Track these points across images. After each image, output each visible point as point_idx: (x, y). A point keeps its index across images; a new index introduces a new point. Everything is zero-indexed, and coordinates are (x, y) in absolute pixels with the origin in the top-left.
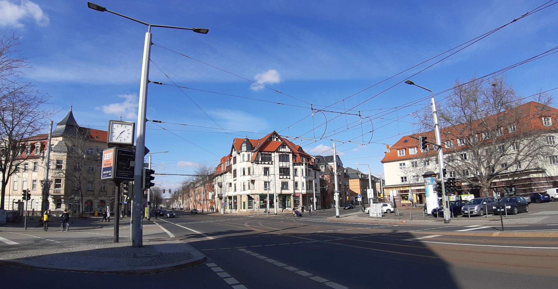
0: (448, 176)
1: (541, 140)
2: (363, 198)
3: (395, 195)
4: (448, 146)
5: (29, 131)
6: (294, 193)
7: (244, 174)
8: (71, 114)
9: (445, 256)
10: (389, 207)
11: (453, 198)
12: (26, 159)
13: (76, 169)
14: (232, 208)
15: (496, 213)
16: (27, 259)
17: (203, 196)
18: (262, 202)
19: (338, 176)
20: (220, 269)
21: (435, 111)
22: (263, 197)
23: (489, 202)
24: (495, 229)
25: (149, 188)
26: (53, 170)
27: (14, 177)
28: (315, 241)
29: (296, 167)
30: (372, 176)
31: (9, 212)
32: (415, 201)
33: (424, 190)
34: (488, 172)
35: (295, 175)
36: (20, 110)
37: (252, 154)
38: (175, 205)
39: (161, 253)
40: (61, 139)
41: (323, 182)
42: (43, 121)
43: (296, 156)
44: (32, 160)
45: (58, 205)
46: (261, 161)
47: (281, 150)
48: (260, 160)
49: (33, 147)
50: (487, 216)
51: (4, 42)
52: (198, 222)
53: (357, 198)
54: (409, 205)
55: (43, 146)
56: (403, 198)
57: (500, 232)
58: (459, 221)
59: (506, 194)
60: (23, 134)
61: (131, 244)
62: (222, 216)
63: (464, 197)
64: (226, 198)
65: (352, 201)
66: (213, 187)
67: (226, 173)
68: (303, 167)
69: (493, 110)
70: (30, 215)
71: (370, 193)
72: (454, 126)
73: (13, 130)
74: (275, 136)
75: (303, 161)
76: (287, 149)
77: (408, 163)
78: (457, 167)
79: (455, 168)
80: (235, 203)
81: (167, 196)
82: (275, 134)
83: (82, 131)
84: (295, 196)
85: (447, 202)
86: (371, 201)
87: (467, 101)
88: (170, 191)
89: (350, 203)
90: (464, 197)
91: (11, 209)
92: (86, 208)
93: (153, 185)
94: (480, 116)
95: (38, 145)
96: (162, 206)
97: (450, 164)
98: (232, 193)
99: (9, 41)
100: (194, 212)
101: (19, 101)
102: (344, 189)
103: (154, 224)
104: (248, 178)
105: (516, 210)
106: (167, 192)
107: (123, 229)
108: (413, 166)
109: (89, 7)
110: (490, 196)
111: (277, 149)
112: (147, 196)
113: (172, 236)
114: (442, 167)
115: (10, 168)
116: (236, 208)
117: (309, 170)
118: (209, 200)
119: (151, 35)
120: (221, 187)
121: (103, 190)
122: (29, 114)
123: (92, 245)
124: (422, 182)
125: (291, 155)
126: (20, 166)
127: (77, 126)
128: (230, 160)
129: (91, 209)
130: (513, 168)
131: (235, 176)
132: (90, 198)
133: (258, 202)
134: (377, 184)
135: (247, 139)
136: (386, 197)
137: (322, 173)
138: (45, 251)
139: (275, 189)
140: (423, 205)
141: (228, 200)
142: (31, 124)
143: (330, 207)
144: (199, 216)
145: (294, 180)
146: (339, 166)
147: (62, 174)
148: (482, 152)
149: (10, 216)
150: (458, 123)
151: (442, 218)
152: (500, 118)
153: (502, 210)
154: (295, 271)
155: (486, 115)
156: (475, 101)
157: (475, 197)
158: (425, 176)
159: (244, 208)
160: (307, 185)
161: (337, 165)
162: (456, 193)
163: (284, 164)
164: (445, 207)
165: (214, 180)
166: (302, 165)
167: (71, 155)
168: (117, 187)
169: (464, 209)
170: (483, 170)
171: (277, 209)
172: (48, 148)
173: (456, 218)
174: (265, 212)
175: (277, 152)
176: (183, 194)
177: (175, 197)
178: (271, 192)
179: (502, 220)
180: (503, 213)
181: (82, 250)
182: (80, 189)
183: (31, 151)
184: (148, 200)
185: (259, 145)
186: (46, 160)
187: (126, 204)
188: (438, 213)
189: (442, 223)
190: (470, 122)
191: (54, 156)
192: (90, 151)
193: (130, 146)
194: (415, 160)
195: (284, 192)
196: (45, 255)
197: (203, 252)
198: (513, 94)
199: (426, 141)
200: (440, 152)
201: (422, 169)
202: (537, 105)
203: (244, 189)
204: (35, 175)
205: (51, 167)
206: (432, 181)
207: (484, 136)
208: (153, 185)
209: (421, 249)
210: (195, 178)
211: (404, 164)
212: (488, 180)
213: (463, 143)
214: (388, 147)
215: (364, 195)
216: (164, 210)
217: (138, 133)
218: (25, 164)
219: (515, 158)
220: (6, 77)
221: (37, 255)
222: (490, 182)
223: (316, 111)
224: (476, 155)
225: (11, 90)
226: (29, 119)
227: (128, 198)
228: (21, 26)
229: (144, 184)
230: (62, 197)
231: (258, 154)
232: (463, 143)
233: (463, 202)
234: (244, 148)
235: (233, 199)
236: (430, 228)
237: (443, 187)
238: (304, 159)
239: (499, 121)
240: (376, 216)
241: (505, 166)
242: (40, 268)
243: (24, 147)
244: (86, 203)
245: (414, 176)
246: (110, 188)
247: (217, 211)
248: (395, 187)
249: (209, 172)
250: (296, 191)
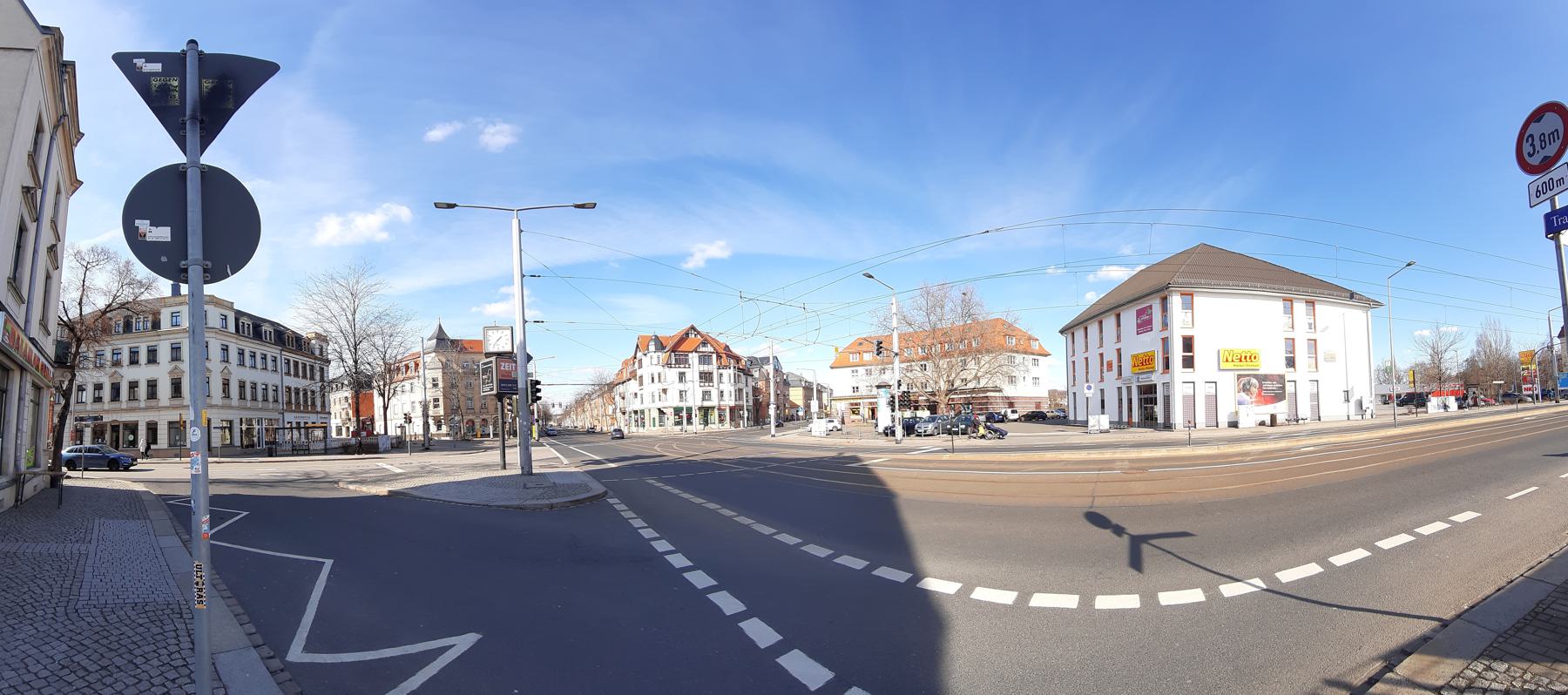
0: (904, 388)
1: (1003, 358)
10: (837, 423)
11: (908, 414)
13: (453, 386)
15: (950, 432)
22: (678, 411)
24: (946, 450)
38: (568, 423)
41: (756, 390)
45: (439, 427)
49: (407, 367)
58: (913, 441)
63: (920, 413)
68: (731, 371)
71: (814, 405)
76: (709, 349)
77: (861, 370)
82: (693, 328)
89: (787, 418)
94: (946, 325)
95: (412, 365)
98: (638, 407)
104: (657, 386)
131: (641, 384)
139: (694, 400)
146: (777, 370)
152: (965, 329)
156: (942, 307)
158: (879, 387)
171: (696, 426)
177: (567, 413)
180: (957, 433)
191: (430, 374)
195: (706, 404)
202: (1004, 323)
215: (807, 406)
219: (975, 374)
228: (384, 236)
234: (652, 348)
243: (398, 369)
246: (492, 404)
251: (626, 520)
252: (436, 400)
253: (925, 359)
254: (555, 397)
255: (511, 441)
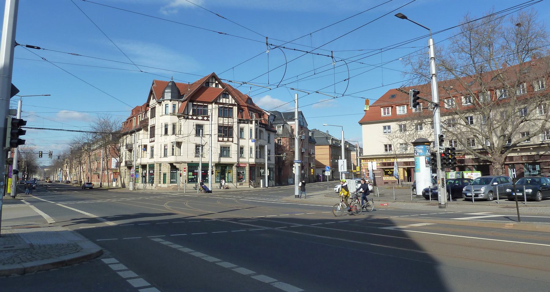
0: (446, 145)
2: (332, 173)
3: (375, 168)
4: (449, 105)
9: (432, 250)
11: (452, 175)
14: (145, 182)
15: (511, 198)
17: (102, 164)
18: (191, 173)
19: (301, 140)
20: (122, 267)
21: (432, 56)
22: (192, 167)
23: (502, 182)
25: (16, 146)
29: (242, 125)
30: (346, 143)
32: (401, 178)
33: (413, 163)
34: (501, 142)
35: (241, 137)
37: (179, 105)
38: (58, 177)
41: (279, 148)
46: (193, 115)
47: (221, 101)
48: (191, 113)
50: (498, 200)
52: (93, 202)
53: (324, 171)
54: (393, 182)
56: (386, 173)
57: (515, 223)
58: (460, 206)
59: (527, 173)
62: (130, 194)
63: (467, 175)
64: (137, 168)
65: (318, 176)
66: (119, 150)
67: (139, 130)
68: (253, 126)
69: (514, 59)
71: (342, 165)
72: (458, 79)
75: (252, 117)
76: (230, 100)
77: (394, 126)
78: (460, 134)
79: (456, 135)
80: (152, 174)
81: (45, 162)
82: (214, 77)
84: (238, 166)
85: (443, 180)
86: (344, 176)
87: (479, 45)
88: (51, 154)
89: (313, 177)
90: (467, 175)
94: (495, 66)
96: (37, 177)
97: (451, 129)
98: (146, 160)
100: (88, 188)
102: (308, 159)
103: (22, 203)
105: (539, 196)
106: (45, 157)
108: (401, 130)
110: (504, 175)
111: (216, 99)
112: (12, 161)
114: (439, 133)
116: (152, 181)
118: (112, 170)
120: (130, 151)
124: (412, 152)
125: (235, 109)
128: (146, 112)
130: (538, 138)
131: (152, 135)
133: (185, 174)
135: (173, 82)
136: (364, 171)
137: (278, 135)
139: (211, 156)
140: (412, 183)
141: (140, 170)
143: (288, 184)
144: (95, 192)
145: (238, 144)
146: (303, 126)
148: (495, 116)
150: (464, 75)
151: (435, 202)
153: (521, 194)
154: (233, 268)
155: (504, 65)
156: (490, 45)
157: (483, 175)
158: (416, 144)
159: (164, 182)
162: (457, 168)
163: (226, 121)
164: (440, 186)
165: (121, 140)
166: (251, 123)
169: (466, 190)
170: (495, 139)
173: (455, 202)
175: (216, 103)
176: (71, 160)
177: (58, 164)
178: (205, 160)
179: (517, 207)
180: (521, 199)
184: (14, 167)
185: (190, 92)
188: (430, 195)
189: (436, 208)
190: (481, 74)
194: (403, 123)
195: (224, 160)
198: (544, 37)
199: (418, 97)
200: (437, 113)
201: (412, 134)
203: (165, 155)
206: (424, 150)
207: (498, 93)
208: (22, 142)
209: (403, 240)
211: (389, 127)
212: (502, 153)
213: (470, 102)
214: (367, 102)
215: (334, 167)
222: (504, 156)
224: (487, 118)
229: (8, 140)
231: (187, 105)
232: (470, 102)
233: (466, 181)
234: (168, 95)
235: (148, 170)
236: (419, 214)
237: (439, 159)
238: (254, 115)
239: (521, 76)
241: (527, 135)
245: (401, 144)
247: (123, 186)
248: (376, 158)
249: (114, 127)
250: (241, 160)
253: (472, 109)
254: (45, 141)
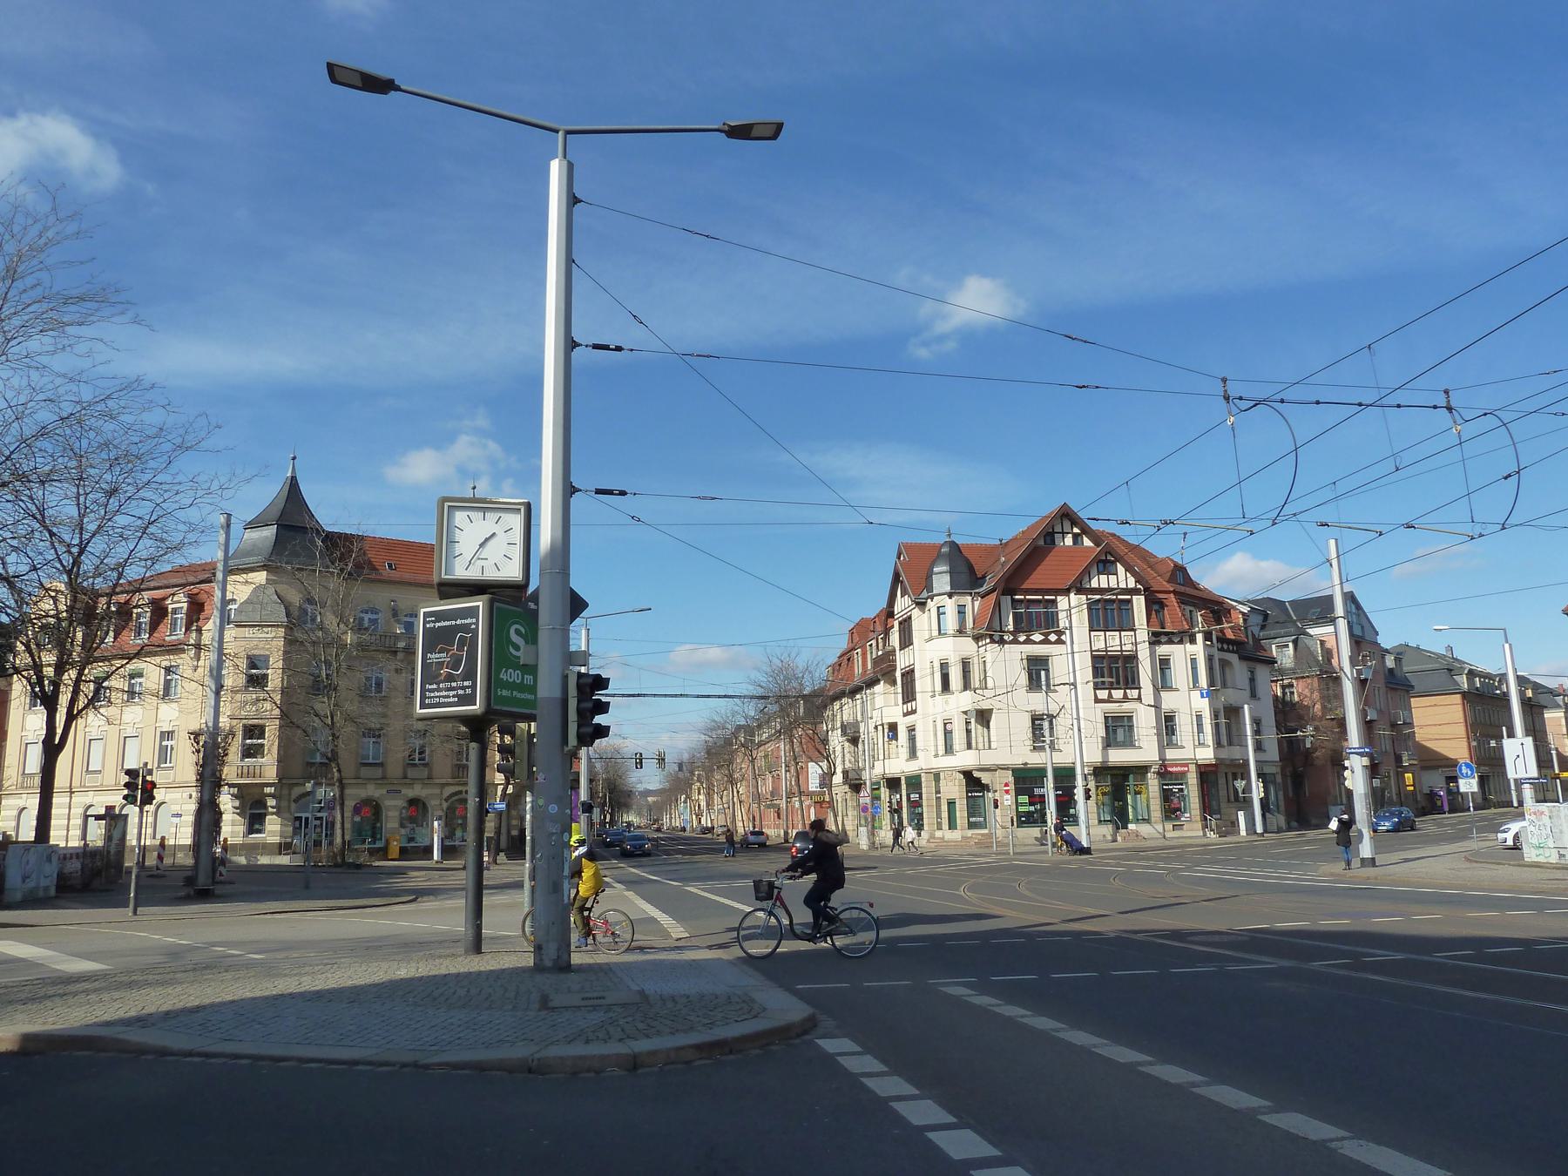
2: (1483, 781)
5: (144, 554)
6: (1163, 759)
7: (946, 686)
8: (293, 486)
12: (138, 655)
13: (319, 687)
16: (141, 1021)
17: (786, 779)
18: (1024, 799)
19: (1362, 683)
20: (869, 1063)
22: (1027, 780)
26: (234, 691)
27: (91, 724)
28: (1270, 963)
29: (1163, 650)
30: (1522, 681)
31: (67, 855)
35: (1163, 682)
36: (108, 477)
37: (972, 605)
38: (680, 818)
39: (642, 993)
40: (261, 577)
41: (1287, 713)
42: (193, 515)
43: (1162, 605)
44: (158, 659)
45: (255, 821)
47: (1094, 584)
49: (159, 611)
51: (16, 229)
53: (1454, 779)
55: (196, 608)
60: (120, 568)
61: (528, 960)
64: (876, 788)
65: (1432, 795)
67: (872, 683)
68: (1198, 649)
70: (151, 861)
71: (1519, 755)
73: (81, 553)
74: (1067, 525)
76: (1122, 578)
80: (915, 805)
81: (648, 780)
82: (1066, 515)
83: (335, 545)
84: (1164, 773)
86: (1528, 792)
88: (661, 760)
89: (1419, 797)
91: (75, 843)
92: (358, 830)
93: (602, 731)
95: (178, 603)
96: (631, 817)
98: (898, 764)
99: (38, 226)
101: (100, 452)
102: (1391, 744)
104: (962, 701)
106: (650, 766)
107: (493, 907)
109: (334, 80)
111: (1080, 579)
113: (677, 930)
115: (76, 692)
117: (1224, 664)
119: (570, 167)
120: (854, 741)
121: (418, 761)
122: (142, 493)
123: (384, 965)
125: (1139, 603)
126: (114, 682)
127: (318, 530)
128: (887, 632)
129: (375, 833)
131: (909, 695)
132: (372, 791)
133: (1008, 800)
134: (1548, 715)
135: (953, 545)
137: (1282, 672)
138: (209, 991)
139: (1080, 746)
141: (884, 793)
142: (152, 529)
145: (1157, 706)
146: (1363, 640)
147: (268, 705)
149: (74, 866)
159: (952, 825)
160: (1217, 727)
161: (1351, 635)
163: (1114, 642)
165: (828, 713)
166: (1193, 641)
167: (299, 635)
168: (473, 745)
172: (216, 613)
174: (1041, 841)
175: (1080, 591)
177: (679, 786)
178: (1063, 758)
181: (349, 983)
182: (333, 757)
183: (154, 626)
184: (583, 795)
185: (1006, 562)
186: (208, 658)
187: (500, 813)
192: (367, 617)
193: (518, 588)
195: (1118, 757)
196: (212, 1005)
197: (799, 995)
203: (949, 749)
204: (168, 715)
205: (228, 682)
210: (751, 710)
215: (1491, 764)
216: (638, 832)
217: (545, 536)
218: (132, 676)
220: (44, 360)
221: (180, 1005)
223: (1244, 405)
225: (67, 408)
226: (144, 510)
227: (510, 790)
230: (268, 790)
231: (998, 604)
234: (942, 582)
240: (1554, 859)
242: (190, 1054)
243: (125, 613)
244: (357, 810)
250: (1171, 754)
251: (882, 1105)
252: (255, 731)
255: (500, 870)
